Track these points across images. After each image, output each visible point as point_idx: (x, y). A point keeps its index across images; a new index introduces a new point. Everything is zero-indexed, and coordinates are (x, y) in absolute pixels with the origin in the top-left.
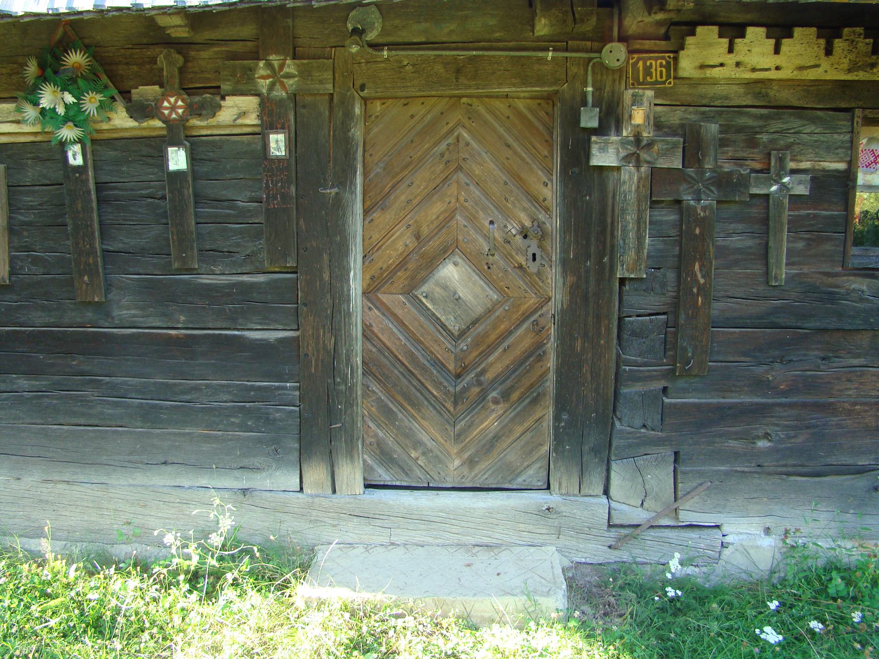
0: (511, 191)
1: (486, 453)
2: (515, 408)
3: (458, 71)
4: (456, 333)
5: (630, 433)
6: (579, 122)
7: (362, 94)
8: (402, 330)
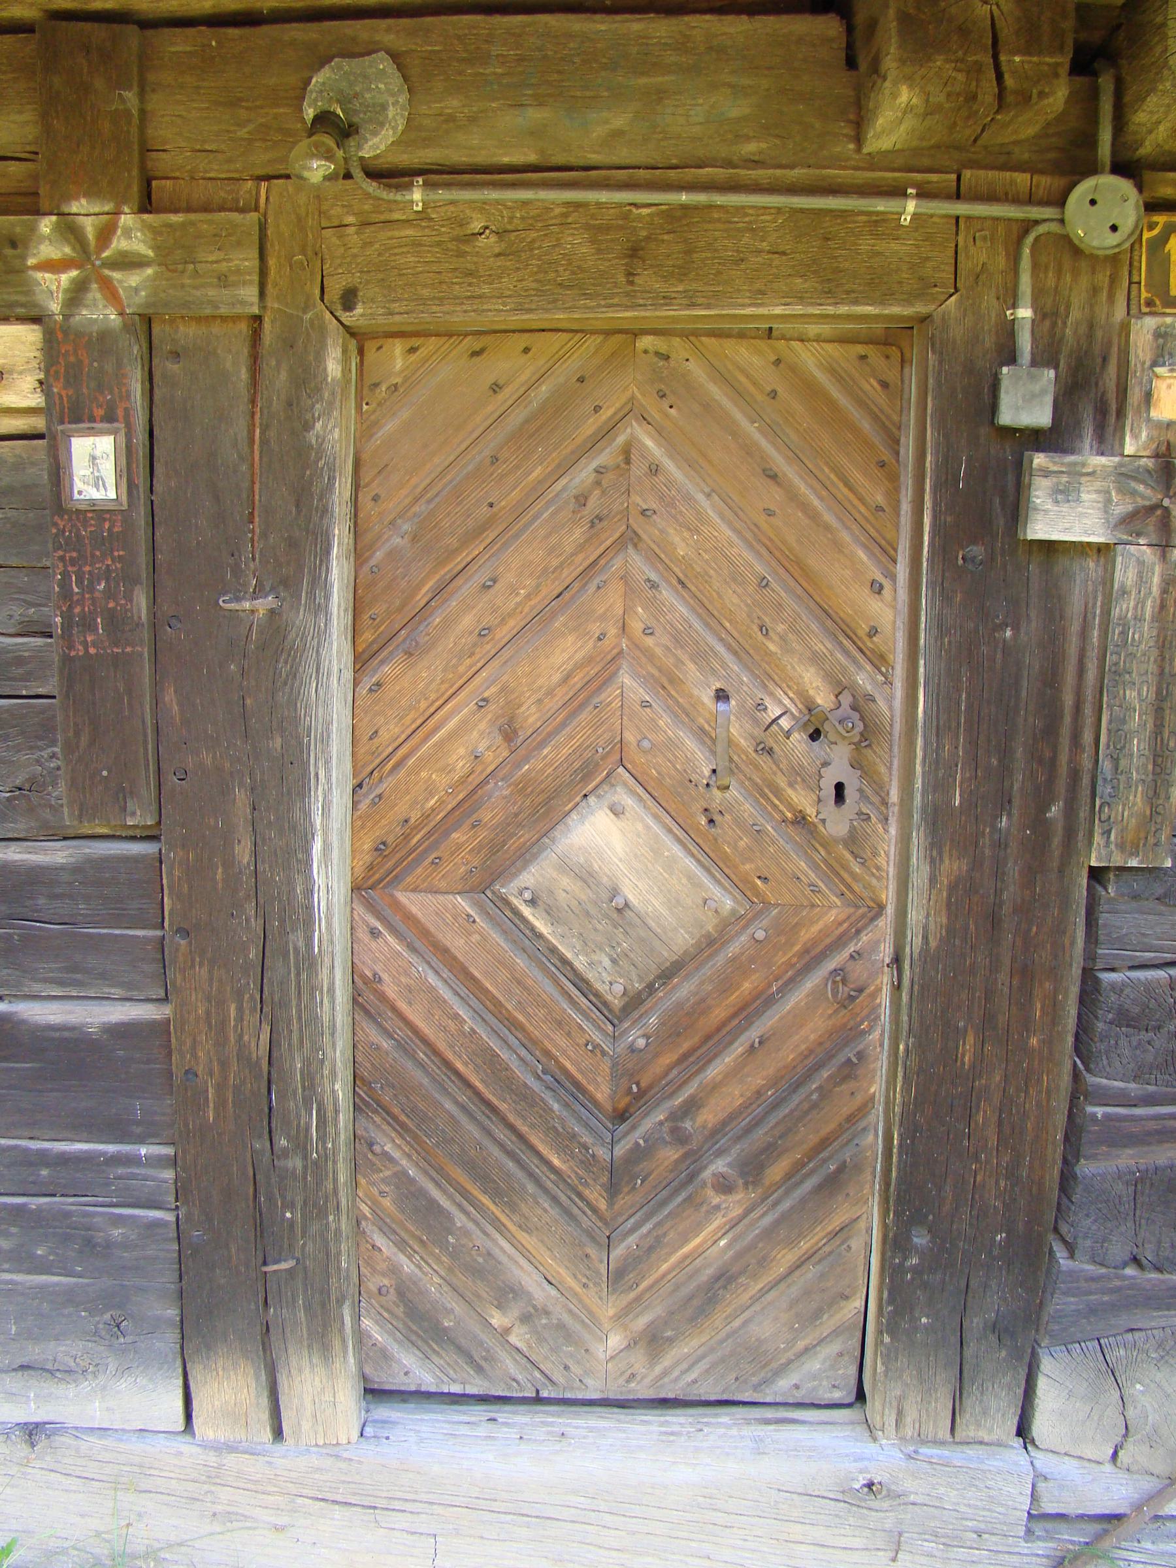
0: (780, 606)
1: (693, 1319)
2: (776, 1204)
3: (634, 252)
4: (617, 1003)
5: (1093, 1279)
6: (994, 408)
7: (347, 318)
8: (463, 991)
